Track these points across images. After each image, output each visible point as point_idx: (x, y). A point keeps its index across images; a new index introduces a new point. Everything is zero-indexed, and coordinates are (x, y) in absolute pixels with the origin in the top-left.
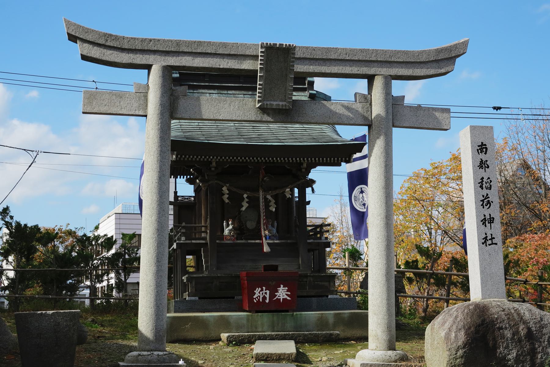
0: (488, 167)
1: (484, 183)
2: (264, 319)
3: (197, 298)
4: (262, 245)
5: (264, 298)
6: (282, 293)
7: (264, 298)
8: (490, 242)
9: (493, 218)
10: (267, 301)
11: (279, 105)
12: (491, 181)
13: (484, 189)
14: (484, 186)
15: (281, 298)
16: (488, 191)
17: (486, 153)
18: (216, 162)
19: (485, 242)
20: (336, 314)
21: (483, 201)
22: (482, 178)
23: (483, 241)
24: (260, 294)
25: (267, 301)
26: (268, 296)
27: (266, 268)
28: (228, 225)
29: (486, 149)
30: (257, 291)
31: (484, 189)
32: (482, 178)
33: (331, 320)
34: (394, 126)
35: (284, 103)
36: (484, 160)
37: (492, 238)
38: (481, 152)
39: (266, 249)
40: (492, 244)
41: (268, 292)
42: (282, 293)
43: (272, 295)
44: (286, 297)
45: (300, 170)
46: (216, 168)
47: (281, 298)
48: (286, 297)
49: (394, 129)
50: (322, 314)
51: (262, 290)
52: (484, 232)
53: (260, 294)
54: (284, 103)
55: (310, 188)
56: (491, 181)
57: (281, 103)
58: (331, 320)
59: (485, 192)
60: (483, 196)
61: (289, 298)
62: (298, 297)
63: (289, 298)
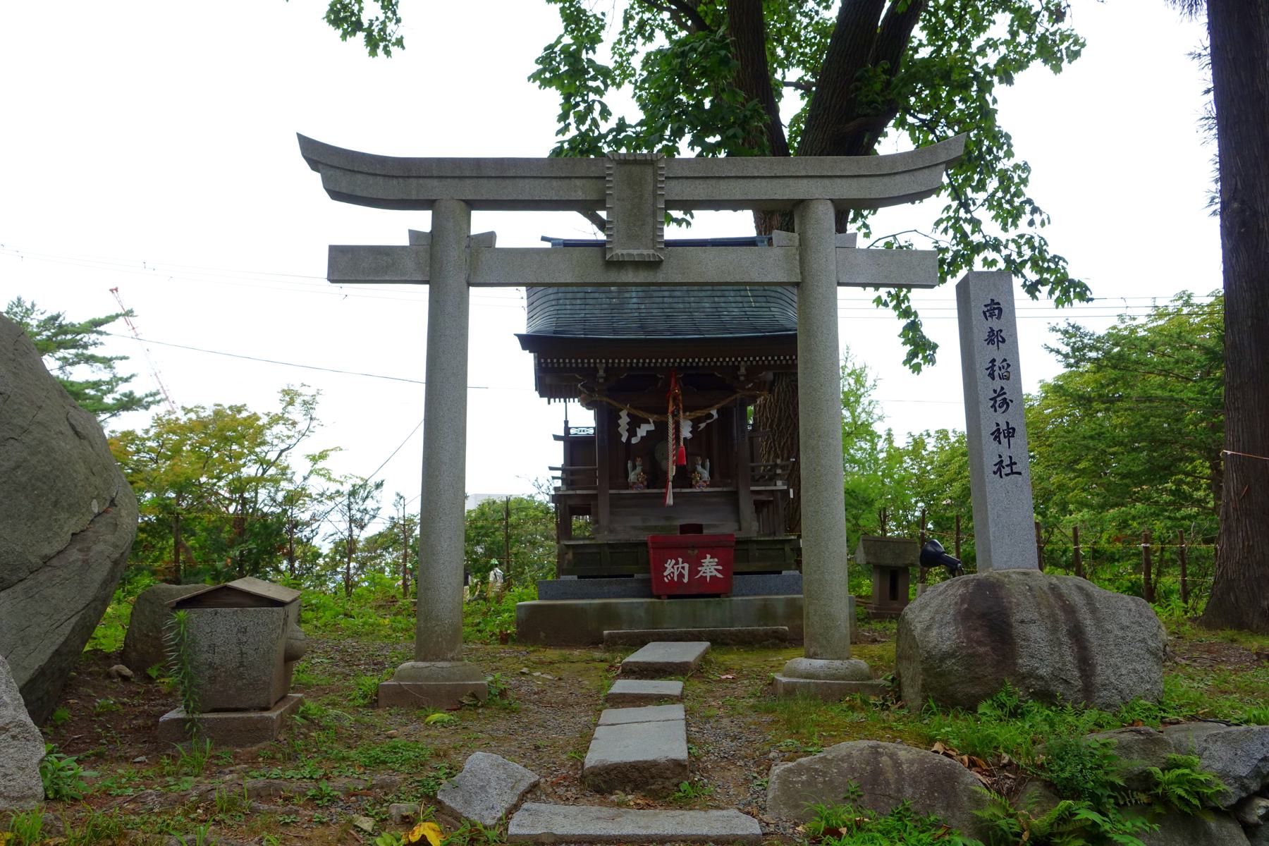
0: (1004, 341)
1: (996, 368)
2: (672, 607)
3: (575, 578)
4: (664, 496)
5: (681, 575)
6: (710, 567)
7: (681, 575)
8: (1008, 470)
9: (1014, 429)
10: (686, 580)
11: (642, 255)
12: (1009, 365)
13: (997, 378)
14: (996, 374)
15: (708, 575)
16: (1003, 383)
17: (999, 318)
18: (606, 370)
19: (999, 469)
20: (788, 600)
21: (994, 399)
22: (994, 361)
23: (995, 468)
24: (674, 569)
25: (686, 580)
26: (686, 573)
27: (685, 529)
28: (634, 468)
29: (1000, 310)
30: (670, 564)
31: (997, 378)
32: (994, 361)
33: (781, 610)
34: (840, 284)
35: (651, 252)
36: (996, 329)
37: (1012, 464)
38: (991, 316)
39: (670, 501)
40: (1013, 473)
41: (686, 565)
42: (710, 567)
43: (693, 572)
44: (715, 573)
45: (736, 378)
46: (606, 379)
47: (708, 575)
48: (715, 573)
49: (840, 289)
50: (766, 600)
51: (677, 563)
52: (997, 453)
53: (674, 569)
54: (651, 252)
55: (896, 444)
56: (1009, 365)
57: (645, 252)
58: (781, 610)
59: (998, 384)
60: (995, 391)
61: (720, 576)
62: (736, 573)
63: (720, 576)
